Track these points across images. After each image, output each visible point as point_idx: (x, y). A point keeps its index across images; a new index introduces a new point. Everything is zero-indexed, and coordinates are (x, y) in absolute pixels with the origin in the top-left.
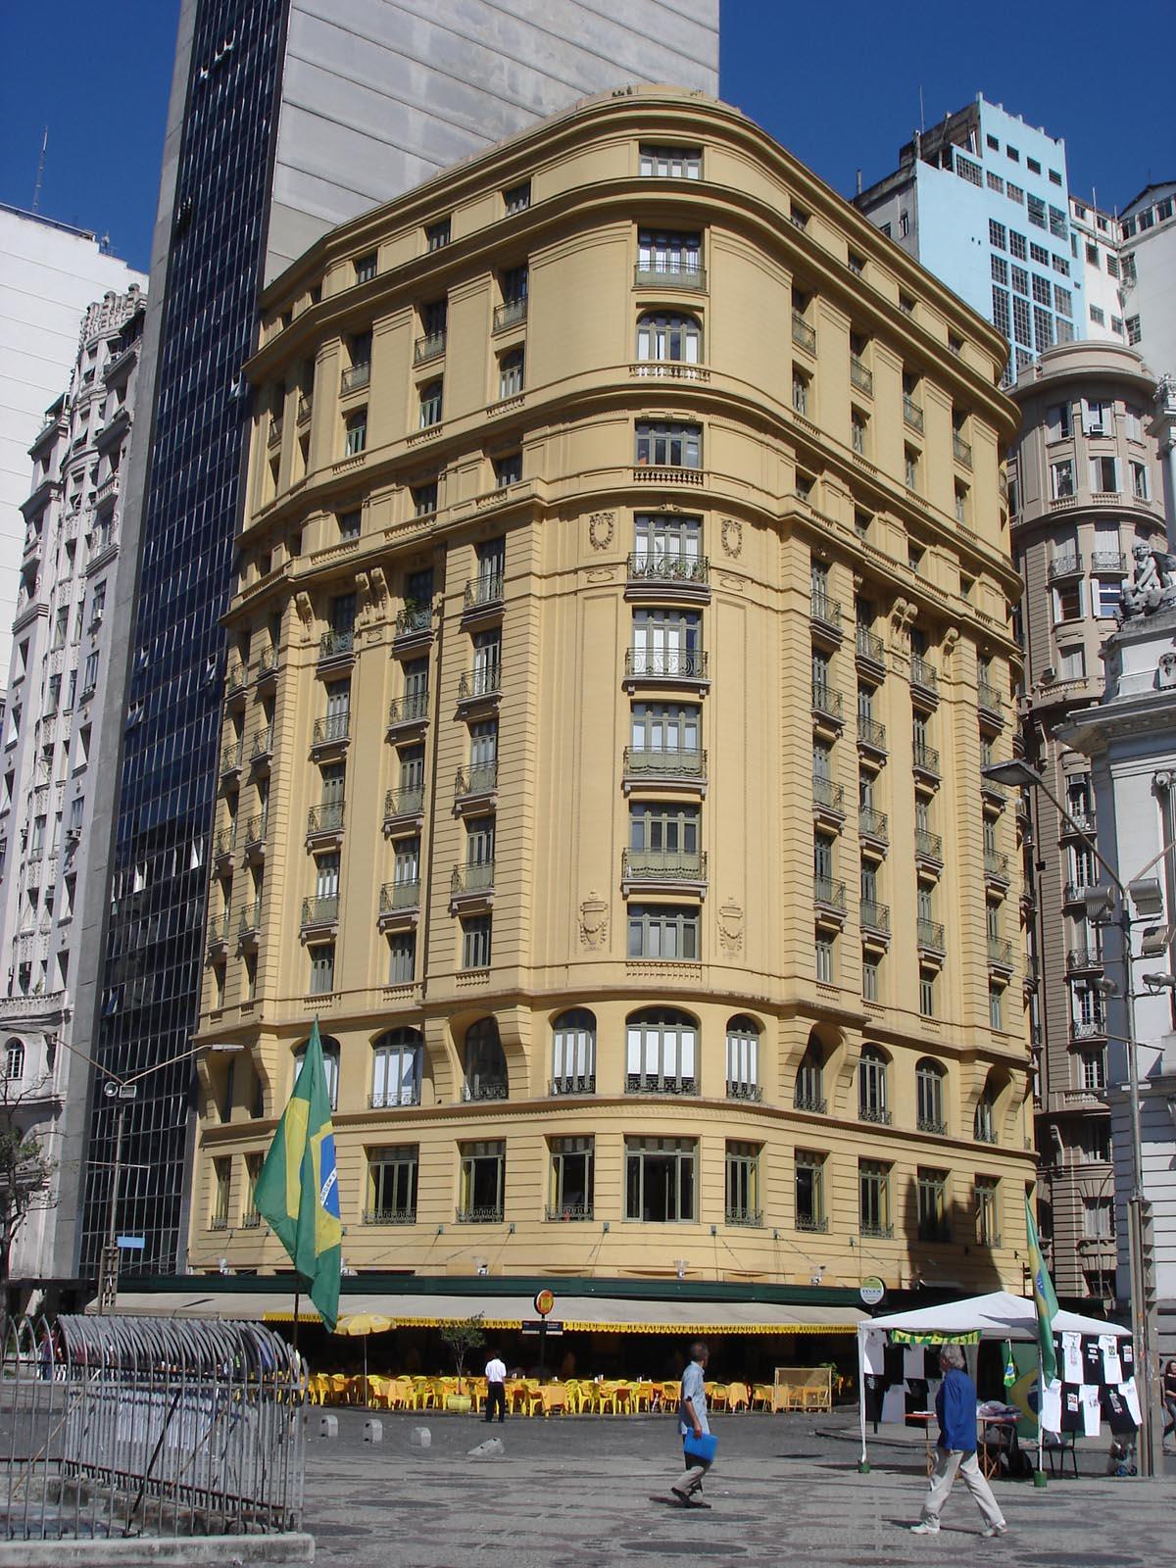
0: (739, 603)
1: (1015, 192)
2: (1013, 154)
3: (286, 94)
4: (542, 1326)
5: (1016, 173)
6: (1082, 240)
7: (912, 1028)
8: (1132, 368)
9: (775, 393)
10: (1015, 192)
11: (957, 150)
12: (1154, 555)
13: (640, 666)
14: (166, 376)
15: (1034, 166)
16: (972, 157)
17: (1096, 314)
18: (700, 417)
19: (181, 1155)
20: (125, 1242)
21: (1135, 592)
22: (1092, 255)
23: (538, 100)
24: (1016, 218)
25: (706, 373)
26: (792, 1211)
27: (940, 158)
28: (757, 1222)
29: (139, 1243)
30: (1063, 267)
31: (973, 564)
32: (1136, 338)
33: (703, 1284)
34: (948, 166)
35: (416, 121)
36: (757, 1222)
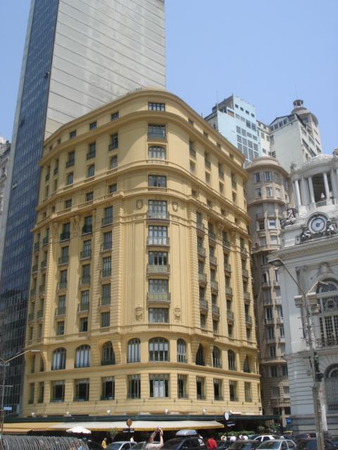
0: (177, 224)
1: (243, 119)
2: (242, 109)
3: (50, 90)
4: (129, 430)
5: (243, 114)
6: (260, 132)
7: (226, 341)
8: (276, 164)
9: (186, 168)
10: (243, 119)
11: (228, 108)
12: (292, 209)
13: (151, 243)
14: (16, 165)
15: (247, 112)
16: (232, 110)
17: (264, 151)
18: (166, 174)
19: (20, 383)
20: (6, 408)
21: (287, 219)
22: (263, 137)
23: (118, 92)
24: (243, 126)
25: (168, 163)
26: (196, 394)
27: (223, 110)
28: (187, 397)
29: (10, 409)
30: (255, 138)
31: (239, 216)
32: (275, 157)
33: (172, 416)
34: (225, 112)
35: (143, 48)
36: (187, 397)
